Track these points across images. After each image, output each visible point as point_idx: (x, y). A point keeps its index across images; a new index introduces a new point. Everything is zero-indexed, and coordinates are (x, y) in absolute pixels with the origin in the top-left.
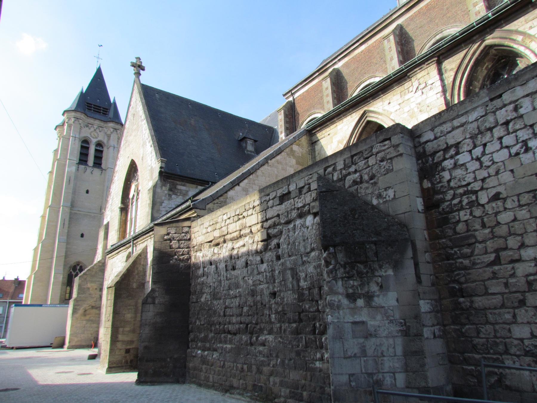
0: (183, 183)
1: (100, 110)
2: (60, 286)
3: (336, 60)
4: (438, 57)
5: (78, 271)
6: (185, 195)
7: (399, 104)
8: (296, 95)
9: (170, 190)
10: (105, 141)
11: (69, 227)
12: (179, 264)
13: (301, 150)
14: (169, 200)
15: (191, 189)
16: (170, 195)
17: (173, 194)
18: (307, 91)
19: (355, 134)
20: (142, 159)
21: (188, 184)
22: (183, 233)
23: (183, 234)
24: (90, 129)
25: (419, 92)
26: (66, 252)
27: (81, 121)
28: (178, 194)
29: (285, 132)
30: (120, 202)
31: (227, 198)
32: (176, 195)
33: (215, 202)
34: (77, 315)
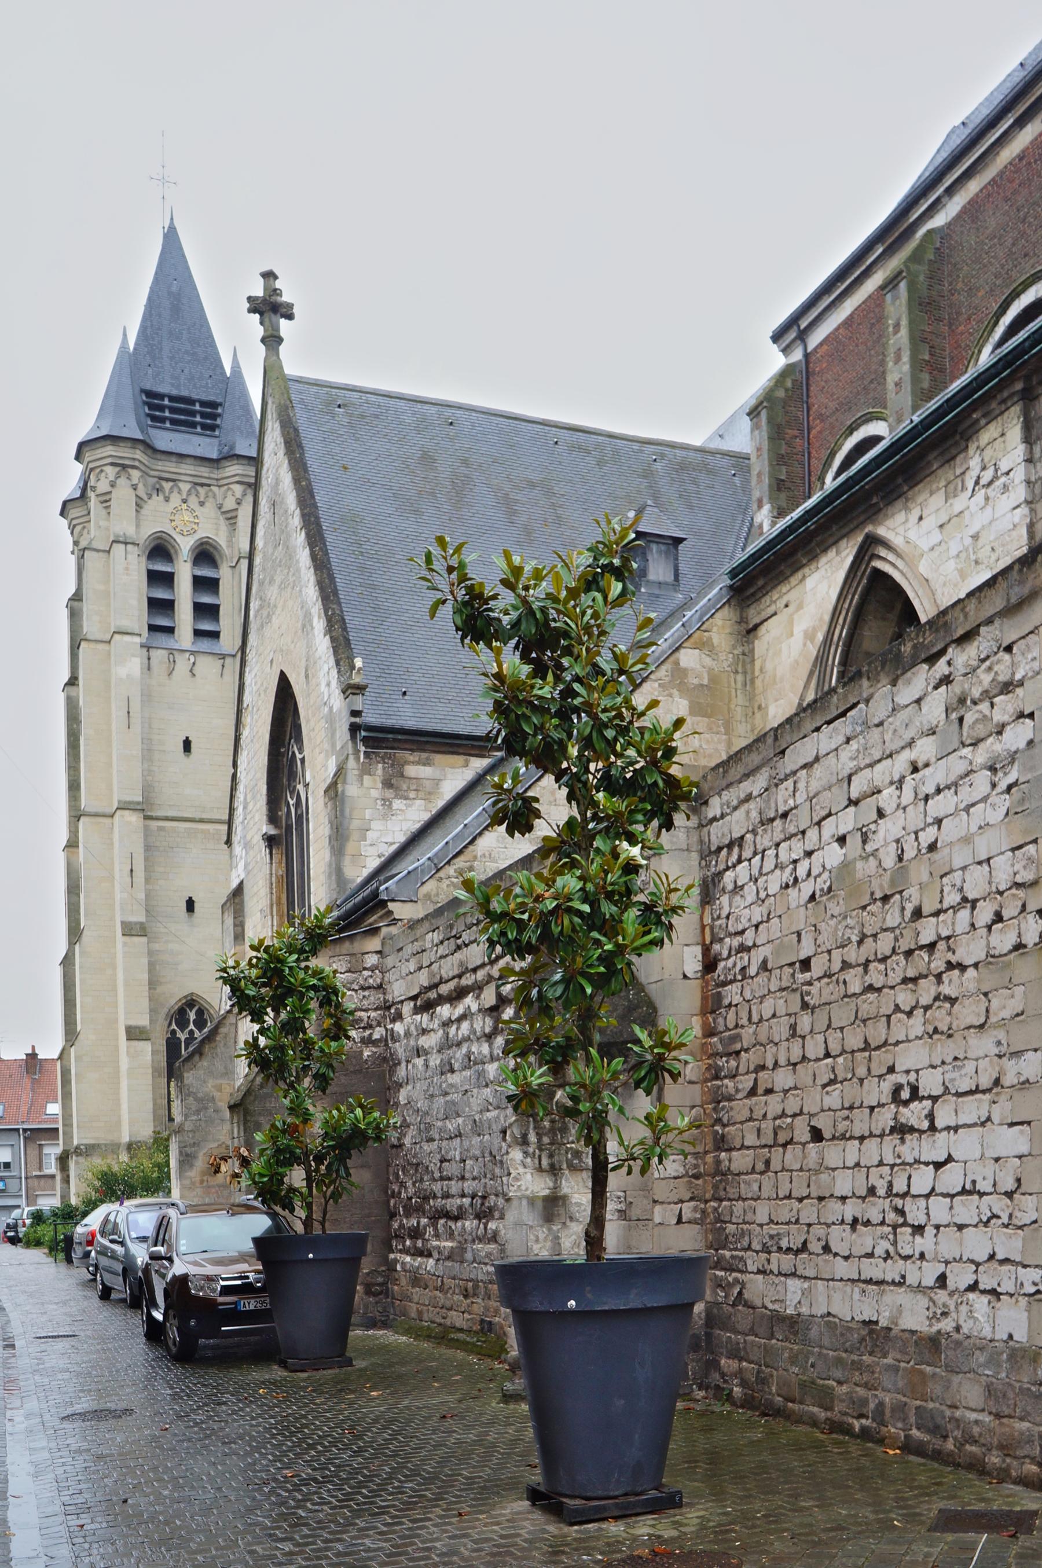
0: (424, 755)
1: (193, 413)
2: (148, 1080)
3: (940, 190)
4: (1027, 378)
5: (192, 1026)
6: (429, 796)
7: (941, 526)
8: (815, 339)
9: (388, 784)
10: (222, 540)
11: (147, 880)
12: (361, 1053)
13: (708, 661)
14: (385, 817)
15: (449, 770)
16: (387, 803)
17: (396, 797)
18: (848, 322)
19: (844, 613)
20: (307, 676)
21: (438, 758)
22: (365, 969)
23: (366, 973)
24: (167, 499)
25: (981, 494)
26: (152, 967)
27: (135, 474)
28: (412, 795)
29: (772, 500)
30: (265, 818)
31: (475, 858)
32: (406, 798)
33: (441, 874)
34: (194, 1173)
